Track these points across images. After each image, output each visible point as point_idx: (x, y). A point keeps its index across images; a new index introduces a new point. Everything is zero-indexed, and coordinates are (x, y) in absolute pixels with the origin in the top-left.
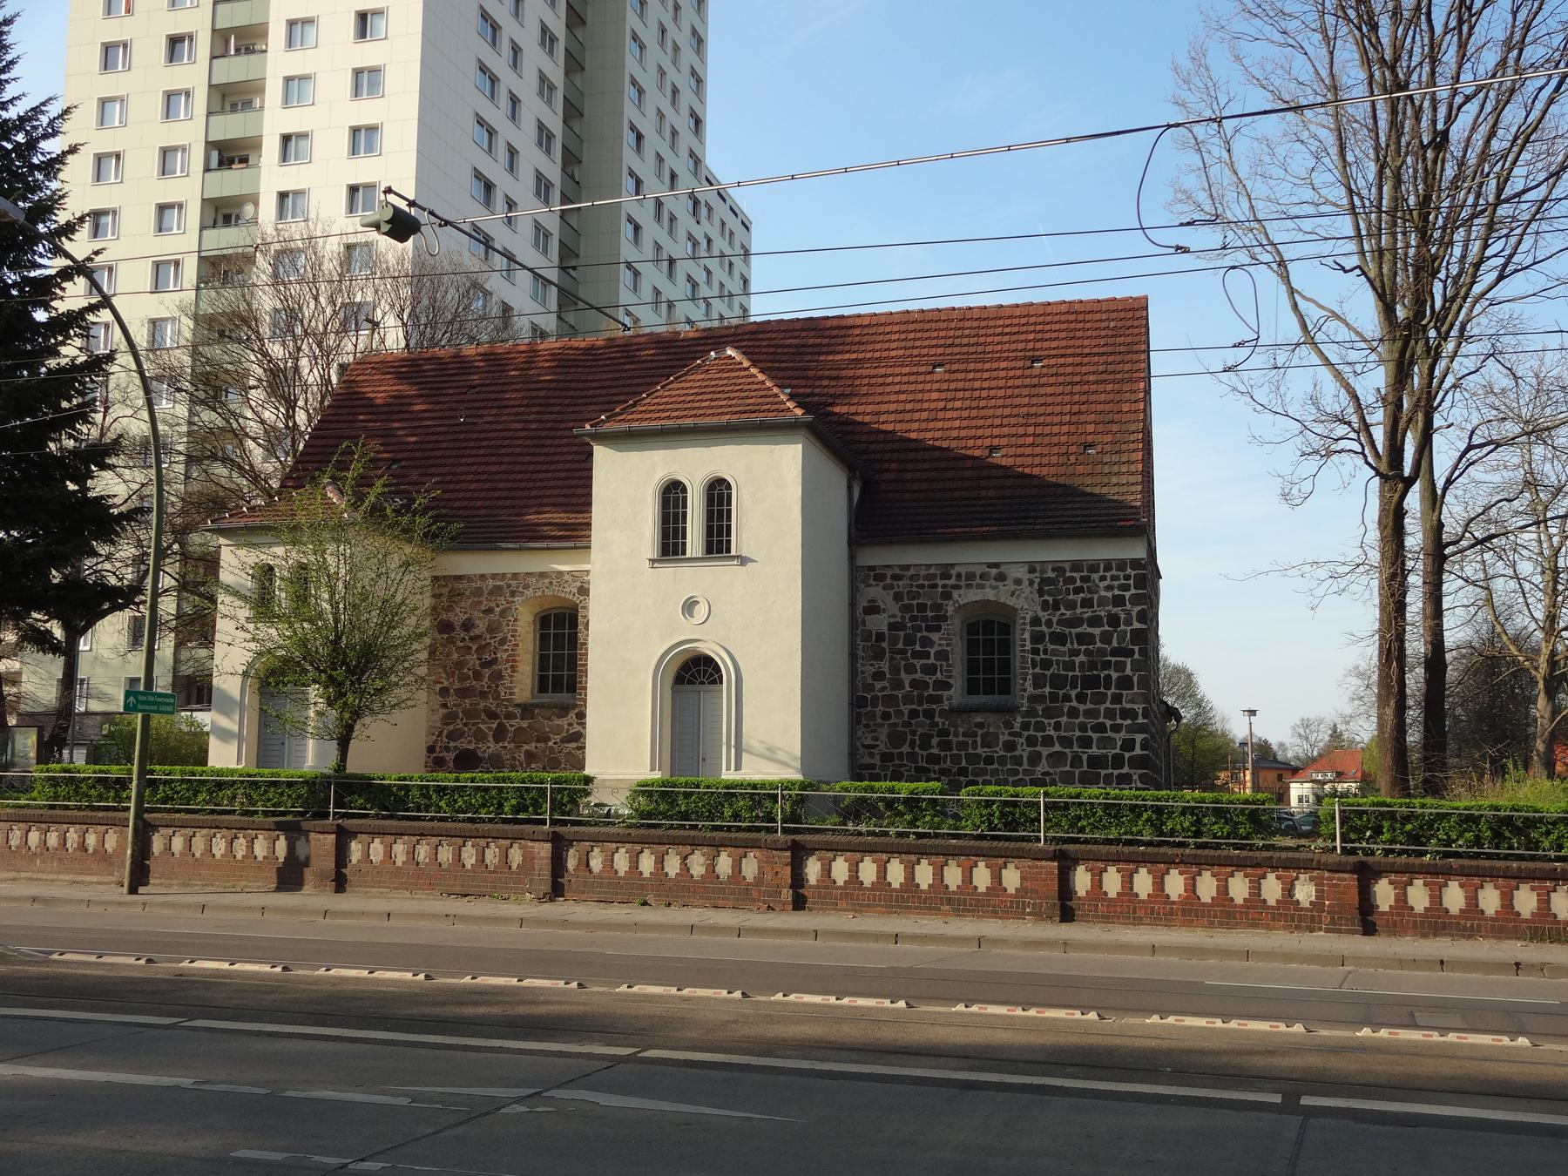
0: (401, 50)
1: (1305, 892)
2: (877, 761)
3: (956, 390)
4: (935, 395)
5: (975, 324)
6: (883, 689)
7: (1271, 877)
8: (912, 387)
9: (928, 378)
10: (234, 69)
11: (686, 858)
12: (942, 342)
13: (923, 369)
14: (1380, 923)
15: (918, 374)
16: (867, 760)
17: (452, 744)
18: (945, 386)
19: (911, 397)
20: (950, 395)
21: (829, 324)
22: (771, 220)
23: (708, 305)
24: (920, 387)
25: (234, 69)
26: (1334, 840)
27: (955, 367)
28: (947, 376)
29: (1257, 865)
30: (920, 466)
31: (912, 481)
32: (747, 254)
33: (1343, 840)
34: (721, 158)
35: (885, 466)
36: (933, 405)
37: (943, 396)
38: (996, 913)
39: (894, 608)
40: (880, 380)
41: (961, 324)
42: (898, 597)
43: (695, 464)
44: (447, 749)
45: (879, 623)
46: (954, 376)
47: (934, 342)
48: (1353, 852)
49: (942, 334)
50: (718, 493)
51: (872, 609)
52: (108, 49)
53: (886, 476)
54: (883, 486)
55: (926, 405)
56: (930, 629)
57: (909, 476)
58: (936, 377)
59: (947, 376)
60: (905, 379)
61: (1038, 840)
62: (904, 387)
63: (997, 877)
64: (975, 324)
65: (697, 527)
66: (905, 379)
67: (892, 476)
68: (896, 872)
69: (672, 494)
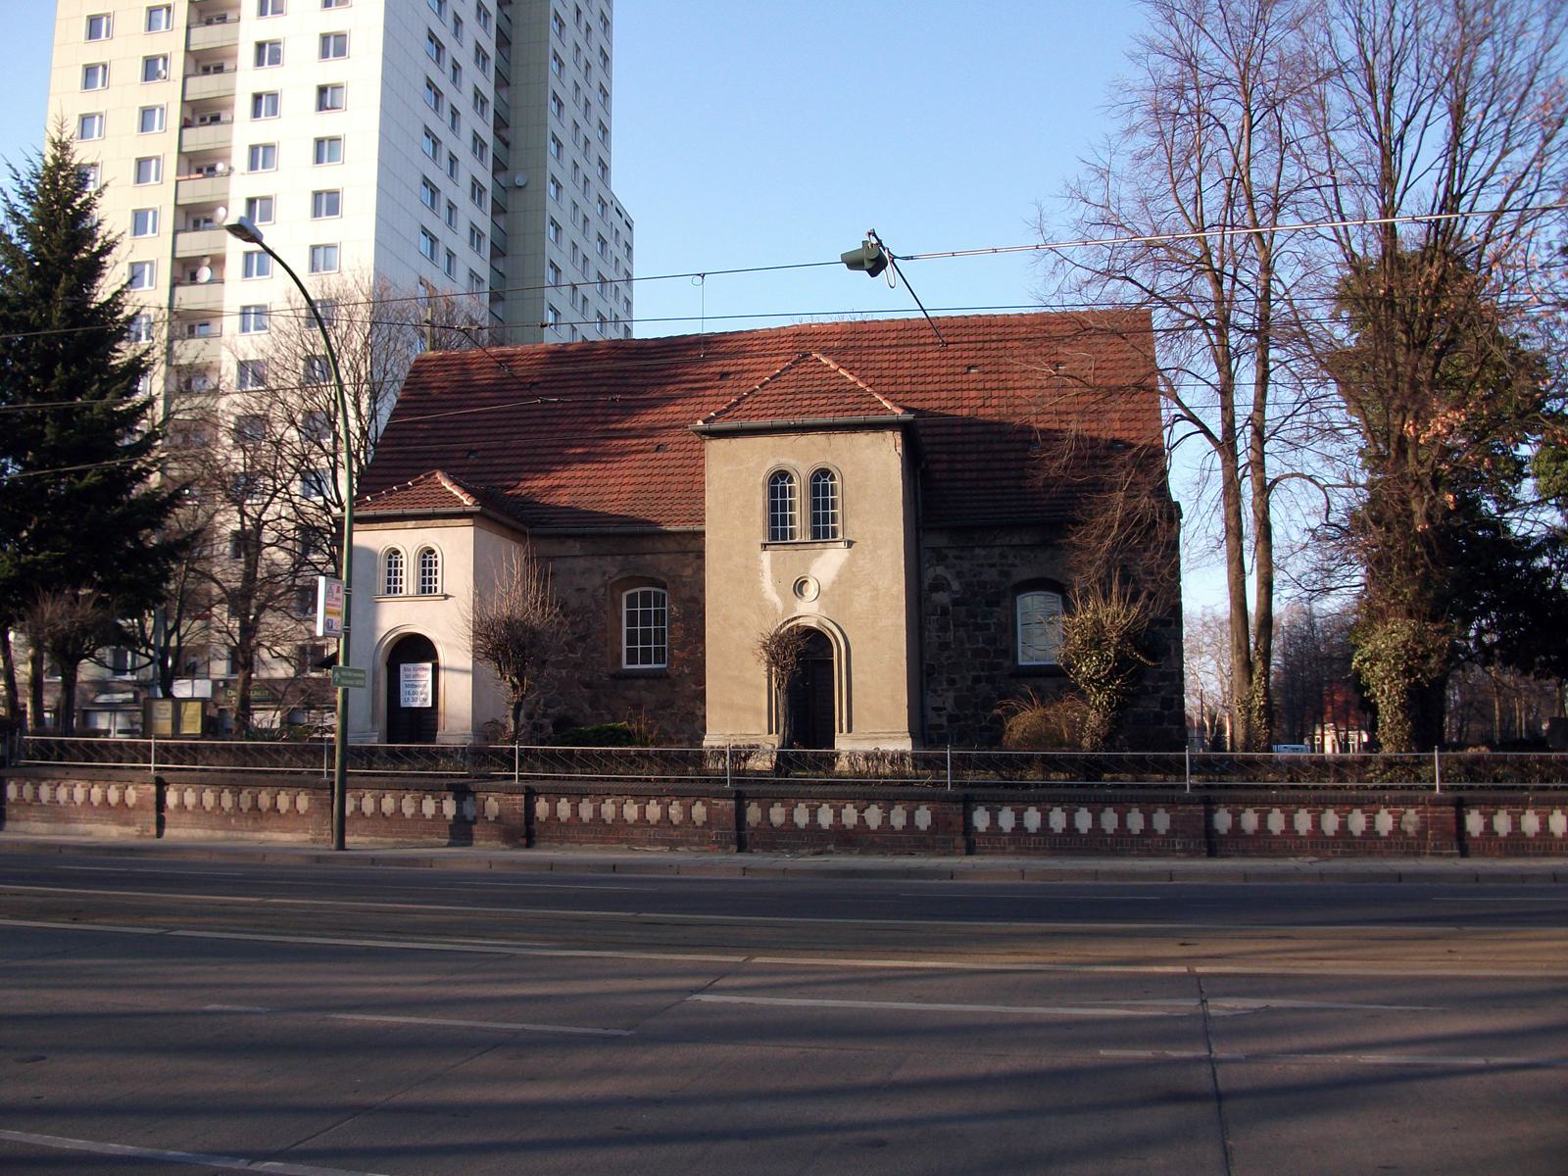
0: (362, 73)
1: (1162, 821)
2: (944, 721)
3: (991, 389)
4: (973, 394)
5: (1001, 330)
6: (949, 658)
7: (1384, 812)
8: (951, 386)
9: (965, 378)
10: (204, 87)
11: (863, 811)
12: (972, 346)
13: (959, 370)
14: (980, 843)
15: (954, 374)
16: (936, 721)
17: (550, 711)
18: (981, 386)
19: (951, 395)
20: (986, 394)
21: (649, 344)
22: (651, 254)
23: (574, 330)
24: (958, 386)
25: (204, 87)
26: (1434, 780)
27: (987, 369)
28: (982, 377)
29: (1264, 803)
30: (967, 457)
31: (962, 471)
32: (629, 279)
33: (1442, 779)
34: (623, 186)
35: (937, 456)
36: (972, 403)
37: (981, 394)
38: (1152, 853)
39: (955, 585)
40: (921, 380)
41: (988, 330)
42: (959, 575)
43: (800, 455)
44: (545, 715)
45: (942, 598)
46: (988, 377)
47: (966, 346)
48: (963, 785)
49: (972, 338)
50: (821, 480)
51: (938, 586)
52: (89, 71)
53: (937, 466)
54: (937, 476)
55: (966, 403)
56: (989, 604)
57: (959, 466)
58: (971, 377)
59: (982, 377)
60: (944, 379)
61: (1185, 787)
62: (944, 386)
63: (994, 819)
64: (1001, 330)
65: (803, 513)
66: (944, 379)
67: (944, 466)
68: (1058, 819)
69: (779, 481)
